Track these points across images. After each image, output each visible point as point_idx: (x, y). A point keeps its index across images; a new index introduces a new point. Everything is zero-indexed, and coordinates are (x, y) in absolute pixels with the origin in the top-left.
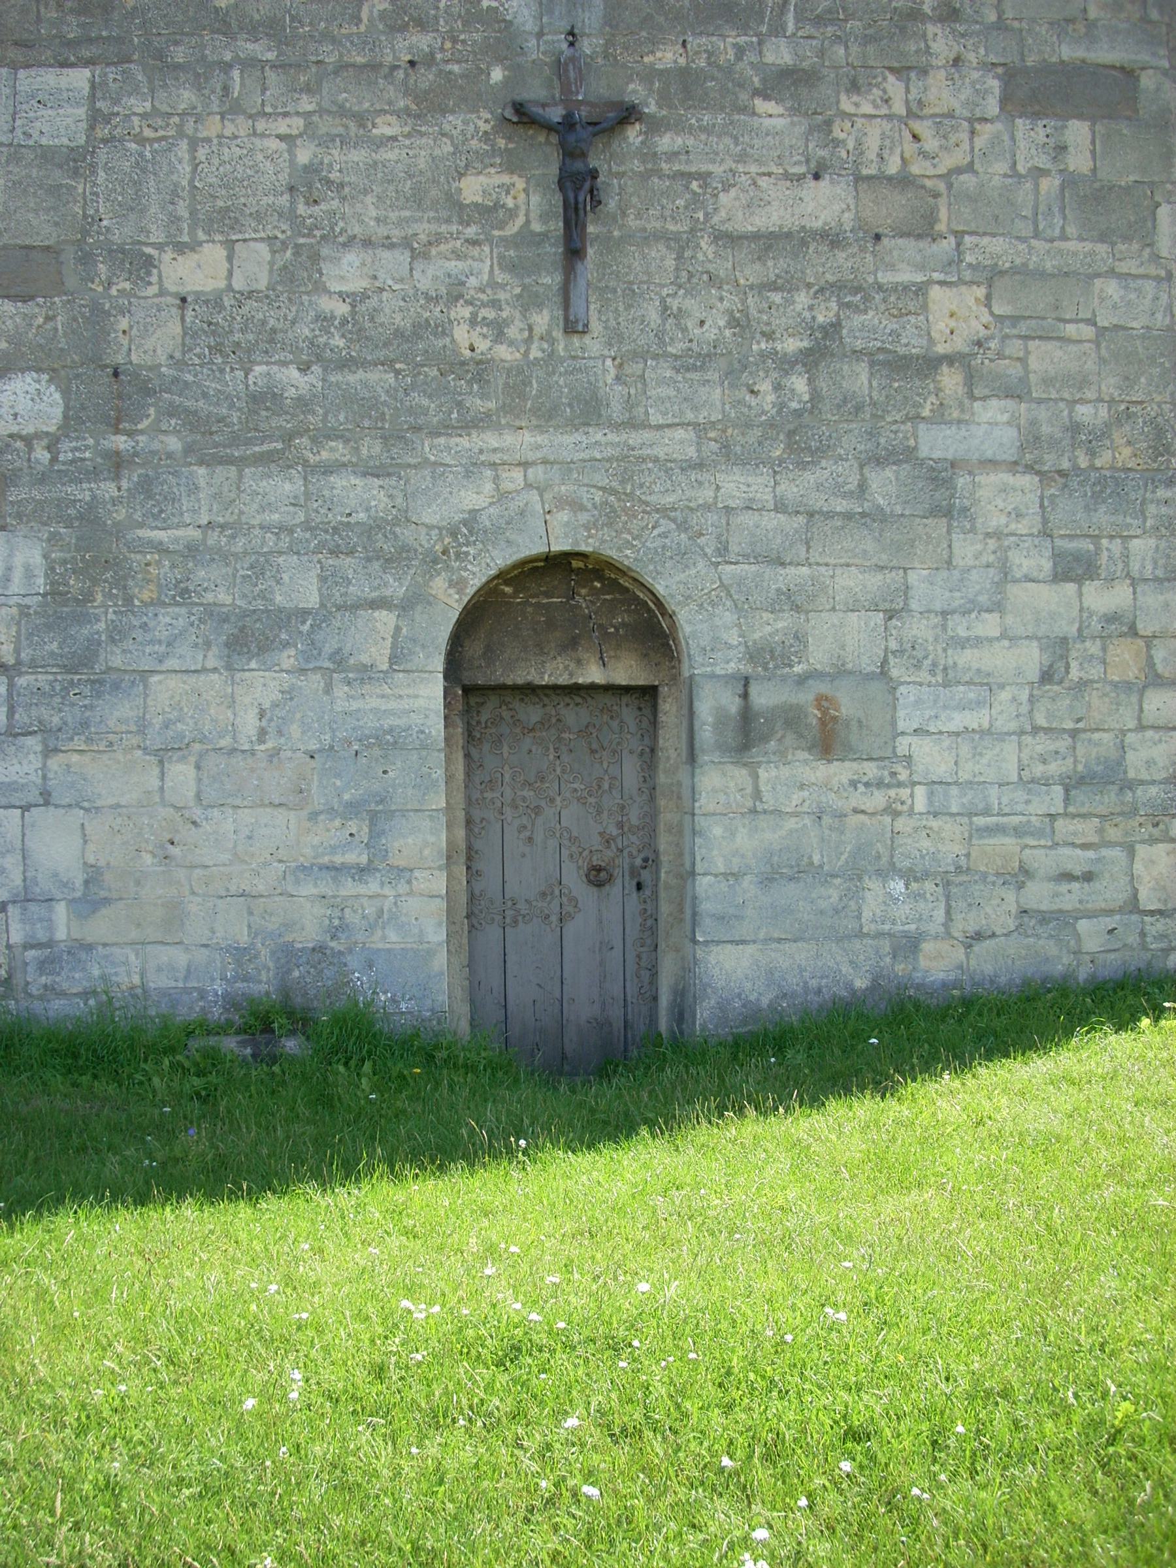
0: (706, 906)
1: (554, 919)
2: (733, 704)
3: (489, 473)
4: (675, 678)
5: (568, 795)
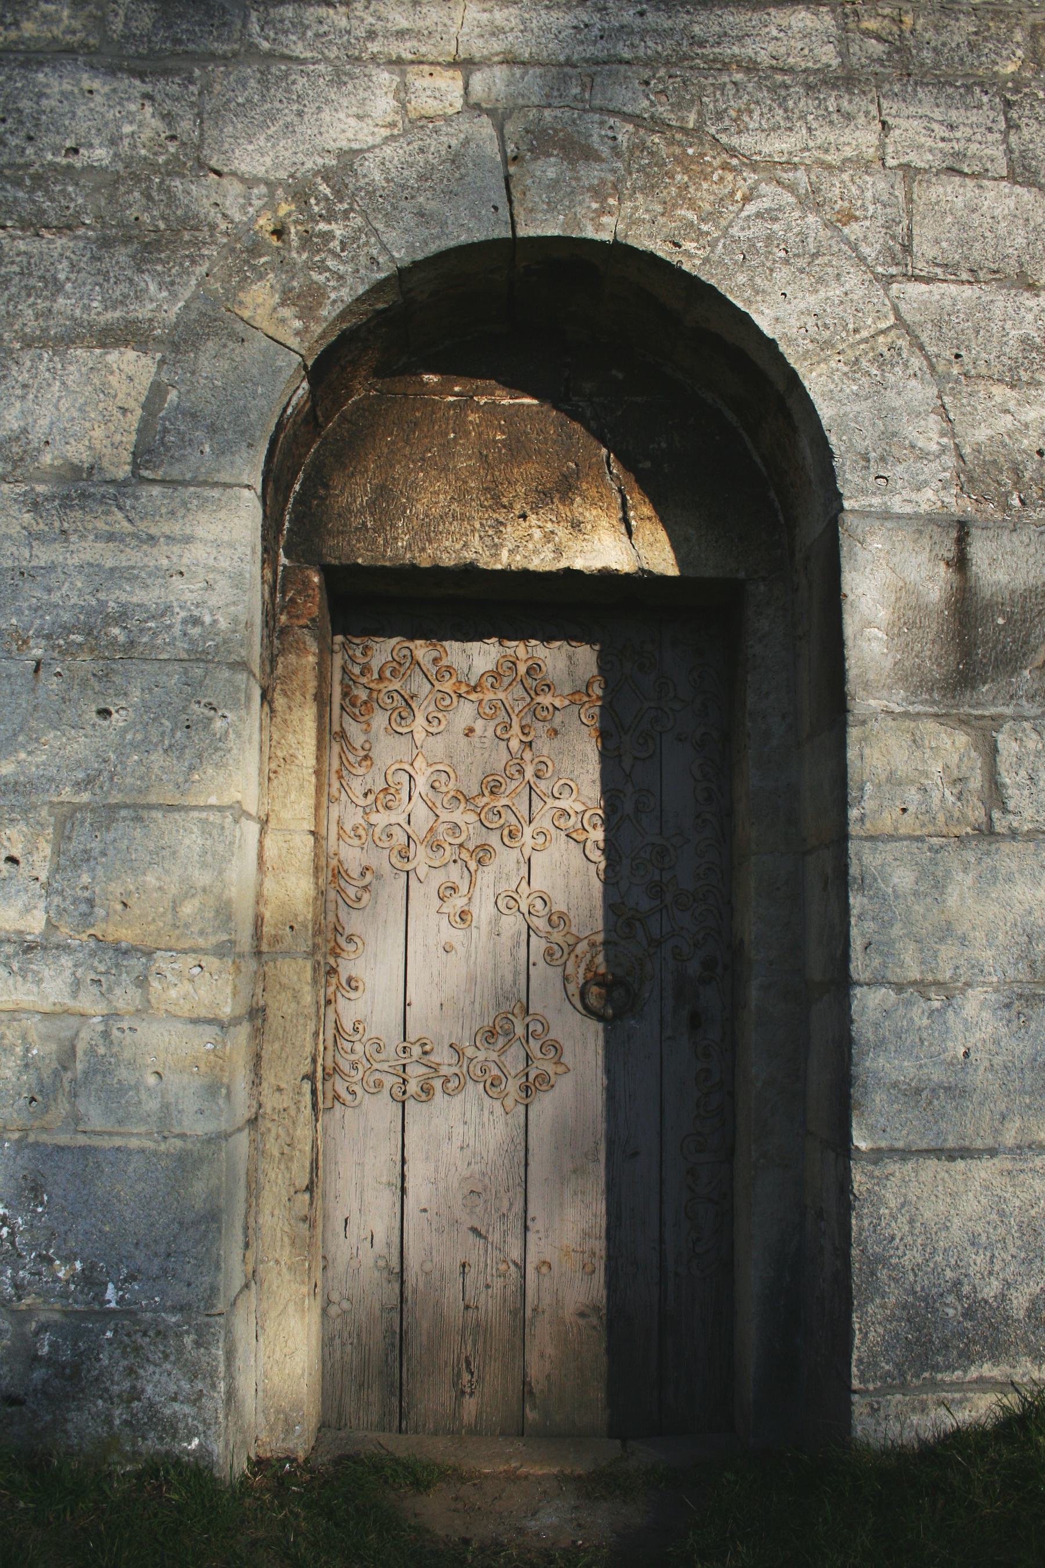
1: (512, 1087)
2: (934, 583)
3: (384, 77)
5: (547, 824)
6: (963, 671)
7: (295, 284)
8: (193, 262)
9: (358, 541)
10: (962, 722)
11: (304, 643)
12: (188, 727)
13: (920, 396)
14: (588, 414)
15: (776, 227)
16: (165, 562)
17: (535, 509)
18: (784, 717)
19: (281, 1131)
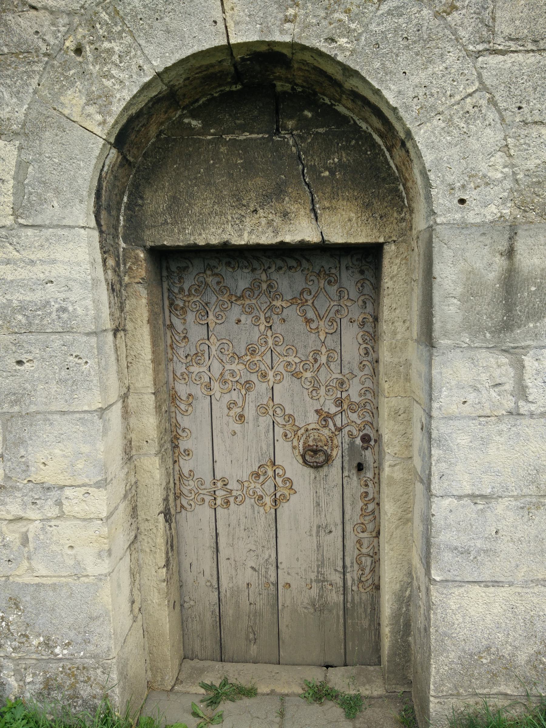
0: (443, 537)
1: (268, 500)
2: (489, 266)
4: (405, 233)
5: (281, 369)
6: (506, 321)
7: (94, 89)
8: (29, 77)
9: (163, 231)
10: (505, 351)
11: (139, 292)
12: (68, 369)
13: (491, 141)
14: (291, 142)
15: (401, 20)
16: (42, 276)
17: (262, 207)
18: (404, 322)
19: (150, 541)
